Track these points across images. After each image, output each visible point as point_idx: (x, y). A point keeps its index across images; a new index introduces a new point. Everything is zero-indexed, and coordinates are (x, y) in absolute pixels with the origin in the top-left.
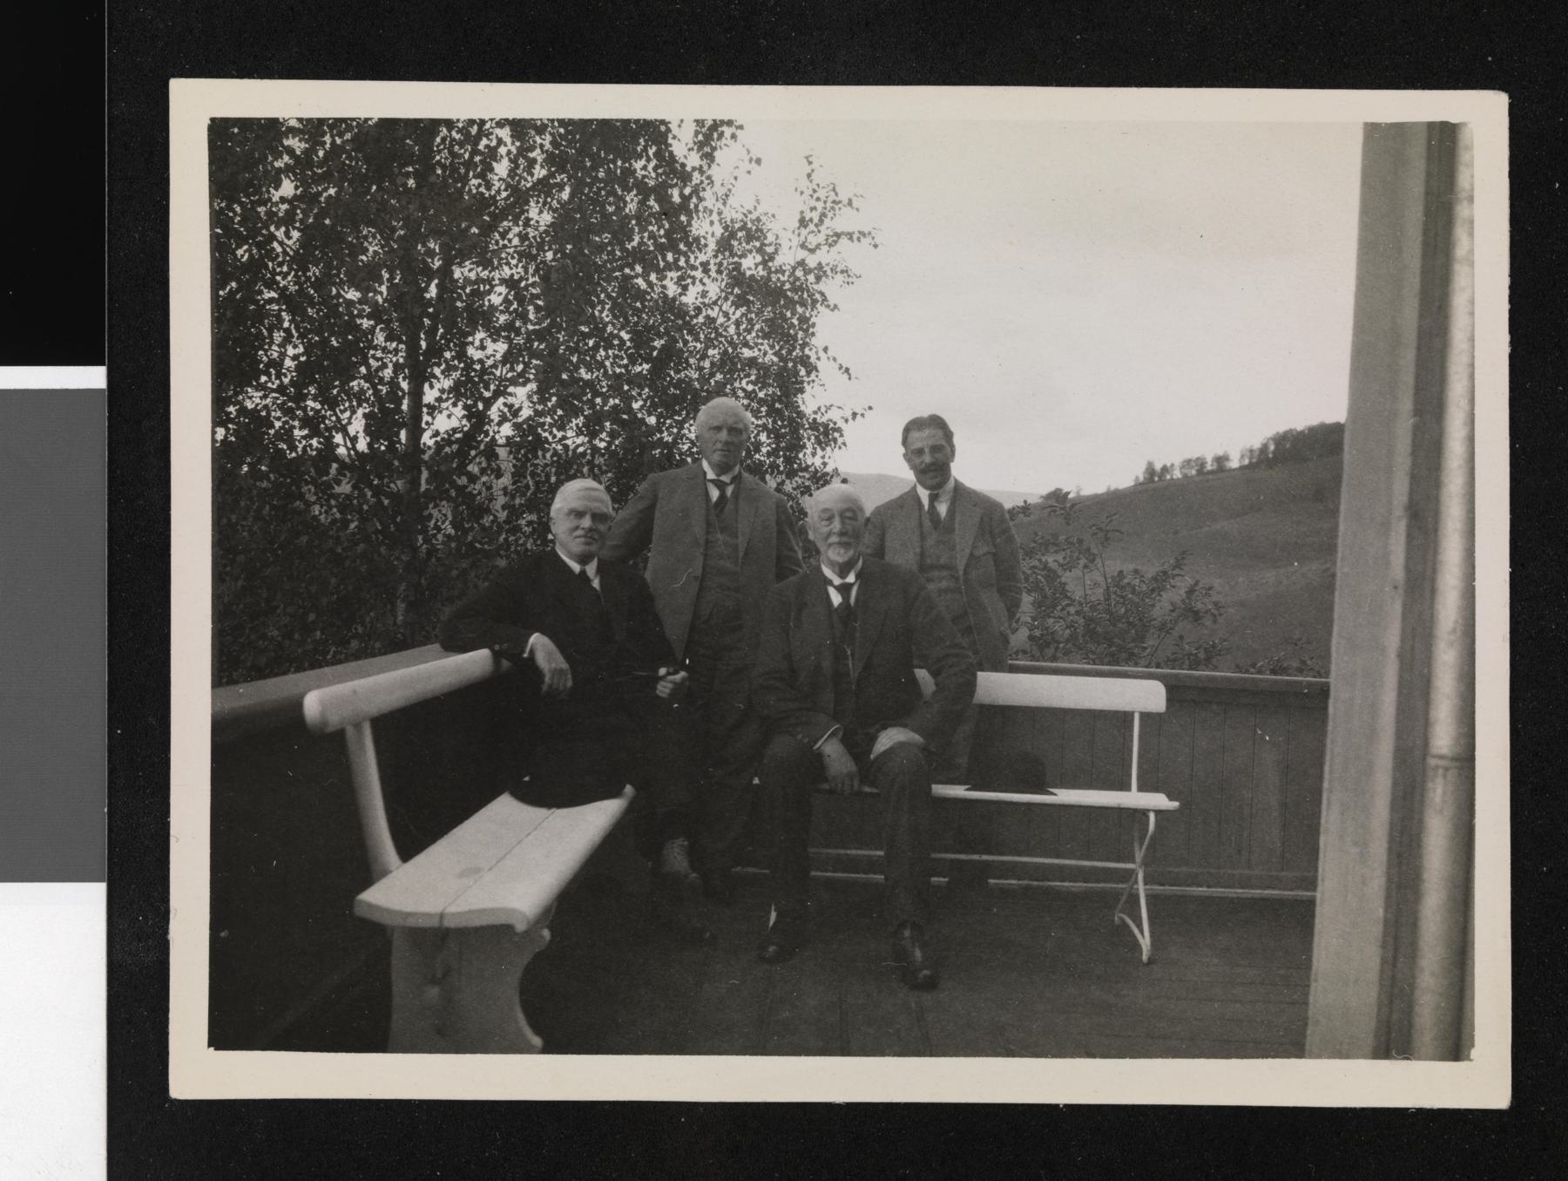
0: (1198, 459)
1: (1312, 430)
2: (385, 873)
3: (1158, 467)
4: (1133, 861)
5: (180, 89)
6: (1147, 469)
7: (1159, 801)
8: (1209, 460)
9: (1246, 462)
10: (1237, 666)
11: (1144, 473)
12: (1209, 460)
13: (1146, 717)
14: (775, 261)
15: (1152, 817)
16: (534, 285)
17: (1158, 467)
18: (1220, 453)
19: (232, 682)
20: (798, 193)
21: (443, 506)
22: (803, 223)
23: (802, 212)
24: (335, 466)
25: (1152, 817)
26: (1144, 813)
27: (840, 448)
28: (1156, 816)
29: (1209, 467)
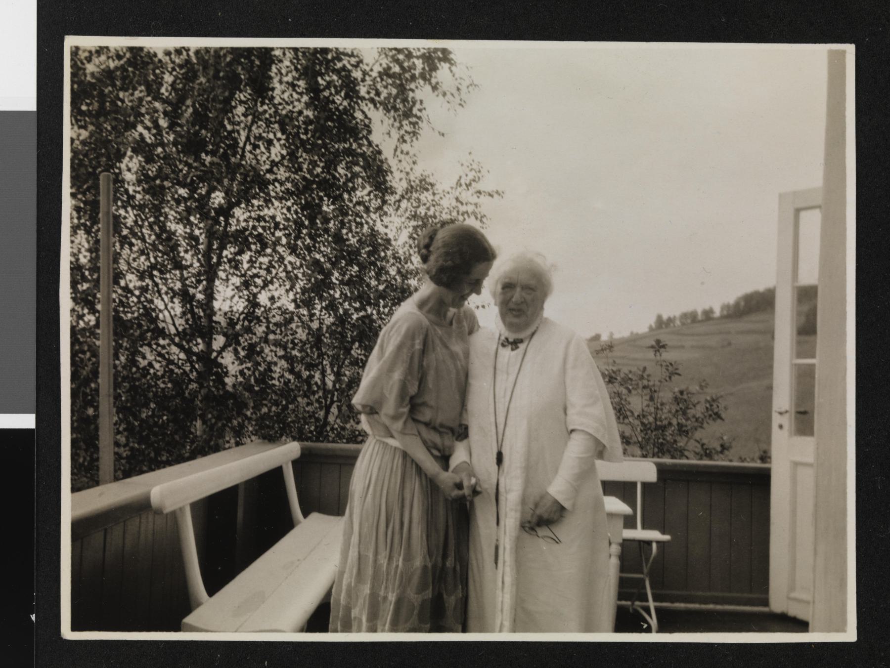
2: (199, 604)
4: (642, 573)
5: (850, 635)
7: (654, 535)
8: (699, 312)
9: (725, 313)
10: (740, 458)
12: (699, 312)
13: (644, 485)
14: (398, 191)
15: (654, 546)
16: (152, 172)
18: (707, 307)
21: (272, 299)
23: (460, 177)
25: (654, 546)
26: (649, 543)
27: (677, 369)
28: (658, 548)
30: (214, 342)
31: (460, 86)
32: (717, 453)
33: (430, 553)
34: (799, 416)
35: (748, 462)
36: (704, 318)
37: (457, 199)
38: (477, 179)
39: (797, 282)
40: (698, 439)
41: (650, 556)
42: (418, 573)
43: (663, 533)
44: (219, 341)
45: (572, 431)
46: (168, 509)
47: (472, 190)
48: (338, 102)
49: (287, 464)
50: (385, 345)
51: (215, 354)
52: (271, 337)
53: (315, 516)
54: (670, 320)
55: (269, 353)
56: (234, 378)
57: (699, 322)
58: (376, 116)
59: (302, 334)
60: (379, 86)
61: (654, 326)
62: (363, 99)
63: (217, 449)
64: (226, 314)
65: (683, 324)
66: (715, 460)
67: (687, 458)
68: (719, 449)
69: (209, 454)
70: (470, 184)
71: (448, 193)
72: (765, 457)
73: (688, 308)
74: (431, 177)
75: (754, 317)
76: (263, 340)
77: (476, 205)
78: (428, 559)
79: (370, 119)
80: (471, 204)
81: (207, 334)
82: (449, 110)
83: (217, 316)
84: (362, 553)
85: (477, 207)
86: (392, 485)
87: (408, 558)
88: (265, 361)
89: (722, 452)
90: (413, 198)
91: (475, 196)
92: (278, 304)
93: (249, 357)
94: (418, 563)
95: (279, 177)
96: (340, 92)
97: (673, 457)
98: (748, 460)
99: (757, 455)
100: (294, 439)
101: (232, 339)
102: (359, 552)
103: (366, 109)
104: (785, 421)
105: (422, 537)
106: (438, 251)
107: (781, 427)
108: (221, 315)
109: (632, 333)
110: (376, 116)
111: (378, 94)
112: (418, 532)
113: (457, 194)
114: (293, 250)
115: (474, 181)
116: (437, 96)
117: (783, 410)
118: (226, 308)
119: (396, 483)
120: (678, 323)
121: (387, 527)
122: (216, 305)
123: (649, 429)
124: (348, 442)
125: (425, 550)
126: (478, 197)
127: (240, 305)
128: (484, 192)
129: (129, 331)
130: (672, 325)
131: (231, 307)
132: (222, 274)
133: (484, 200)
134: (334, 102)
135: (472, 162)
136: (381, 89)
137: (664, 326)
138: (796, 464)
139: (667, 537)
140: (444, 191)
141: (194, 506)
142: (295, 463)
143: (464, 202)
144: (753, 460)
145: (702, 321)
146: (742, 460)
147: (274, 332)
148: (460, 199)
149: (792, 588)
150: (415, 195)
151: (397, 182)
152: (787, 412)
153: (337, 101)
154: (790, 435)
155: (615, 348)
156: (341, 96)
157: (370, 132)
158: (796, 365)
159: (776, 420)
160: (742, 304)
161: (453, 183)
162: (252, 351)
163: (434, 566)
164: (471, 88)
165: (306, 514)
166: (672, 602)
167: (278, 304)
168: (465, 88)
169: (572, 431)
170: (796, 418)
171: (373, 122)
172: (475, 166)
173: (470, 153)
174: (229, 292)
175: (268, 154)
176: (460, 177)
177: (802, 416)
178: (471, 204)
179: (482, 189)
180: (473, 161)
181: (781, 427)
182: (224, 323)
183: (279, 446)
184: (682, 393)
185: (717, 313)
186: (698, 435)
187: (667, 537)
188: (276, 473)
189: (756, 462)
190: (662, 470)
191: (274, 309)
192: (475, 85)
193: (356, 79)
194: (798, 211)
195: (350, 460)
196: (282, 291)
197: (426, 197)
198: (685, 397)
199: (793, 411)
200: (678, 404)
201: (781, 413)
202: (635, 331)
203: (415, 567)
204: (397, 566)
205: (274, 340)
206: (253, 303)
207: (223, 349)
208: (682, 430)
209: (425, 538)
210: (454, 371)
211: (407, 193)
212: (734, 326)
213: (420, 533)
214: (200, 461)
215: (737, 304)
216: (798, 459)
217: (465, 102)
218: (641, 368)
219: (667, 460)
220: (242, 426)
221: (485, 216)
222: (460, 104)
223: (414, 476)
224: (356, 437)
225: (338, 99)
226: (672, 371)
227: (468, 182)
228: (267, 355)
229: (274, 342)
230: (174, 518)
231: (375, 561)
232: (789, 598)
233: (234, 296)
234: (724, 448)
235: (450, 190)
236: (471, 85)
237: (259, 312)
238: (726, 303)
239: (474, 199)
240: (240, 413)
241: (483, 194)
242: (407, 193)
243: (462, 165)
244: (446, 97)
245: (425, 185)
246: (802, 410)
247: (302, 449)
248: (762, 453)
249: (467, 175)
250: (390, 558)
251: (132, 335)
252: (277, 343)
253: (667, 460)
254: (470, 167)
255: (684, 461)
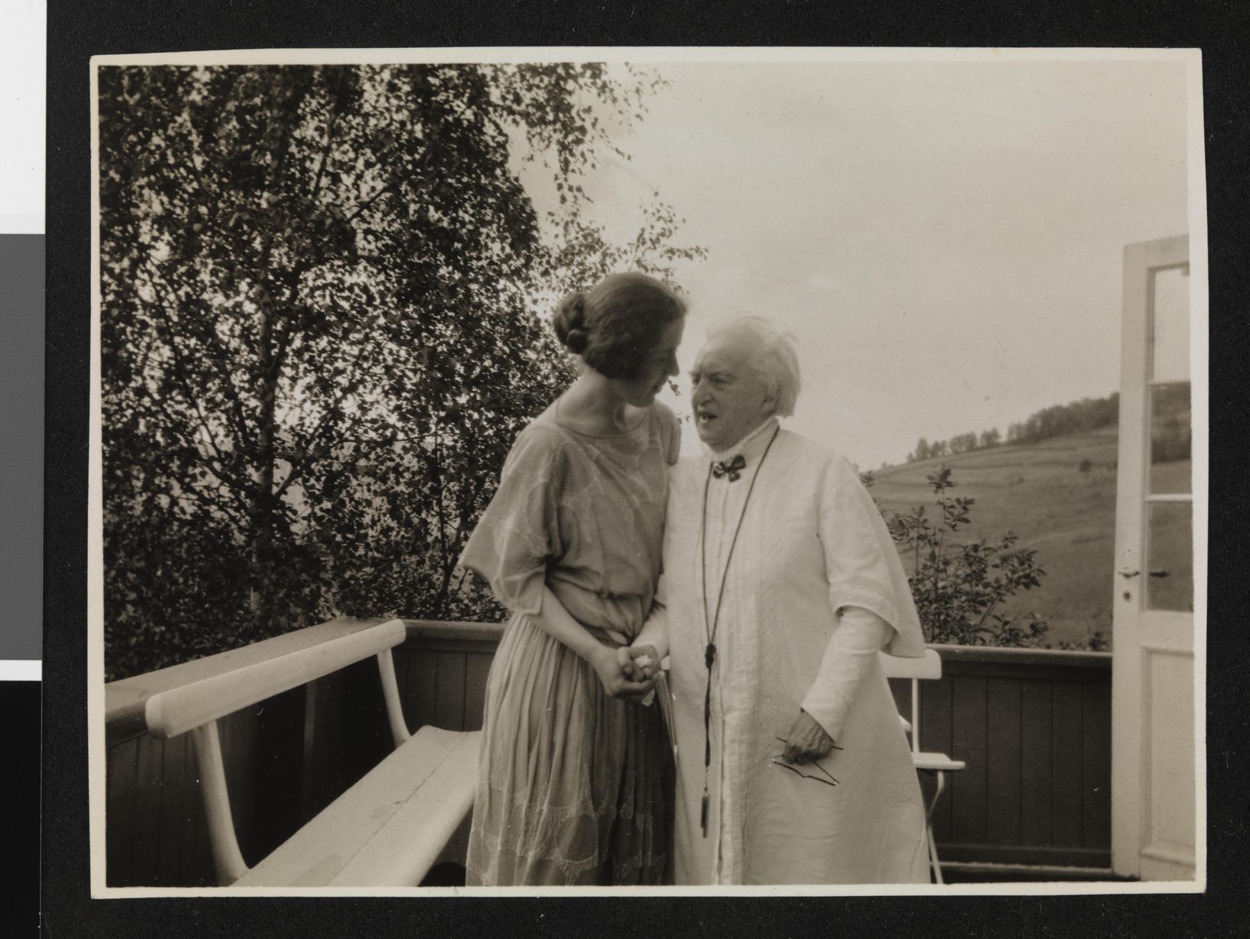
0: (968, 436)
1: (1076, 406)
3: (930, 443)
5: (1197, 884)
6: (920, 447)
8: (979, 435)
9: (1015, 436)
11: (917, 451)
12: (979, 435)
13: (922, 683)
15: (941, 776)
17: (930, 443)
18: (989, 429)
19: (120, 676)
20: (642, 210)
21: (363, 407)
22: (641, 239)
23: (643, 230)
24: (176, 523)
25: (941, 776)
28: (945, 778)
29: (979, 444)
30: (275, 471)
31: (640, 87)
32: (1027, 637)
33: (595, 797)
34: (1154, 579)
35: (1072, 649)
36: (985, 443)
37: (638, 262)
38: (668, 233)
39: (1152, 378)
40: (998, 614)
41: (934, 795)
42: (574, 824)
43: (953, 757)
44: (283, 470)
45: (841, 611)
46: (177, 728)
47: (660, 249)
48: (459, 110)
49: (384, 652)
50: (556, 484)
51: (275, 490)
52: (362, 462)
53: (427, 732)
54: (938, 447)
55: (361, 487)
56: (305, 522)
57: (978, 449)
58: (517, 133)
59: (410, 461)
60: (518, 85)
61: (914, 455)
62: (495, 107)
63: (276, 631)
64: (292, 428)
65: (956, 453)
66: (1022, 646)
67: (984, 642)
68: (1029, 632)
69: (266, 638)
70: (658, 240)
71: (625, 252)
72: (1100, 639)
73: (962, 431)
74: (601, 232)
75: (1056, 443)
76: (349, 467)
77: (666, 270)
78: (591, 807)
79: (506, 135)
80: (659, 270)
81: (265, 459)
82: (621, 123)
83: (281, 431)
84: (494, 787)
85: (667, 275)
86: (540, 681)
87: (557, 801)
88: (352, 499)
89: (1034, 635)
90: (575, 263)
91: (665, 257)
92: (372, 415)
93: (329, 492)
94: (573, 810)
95: (373, 227)
96: (463, 94)
97: (963, 641)
98: (1072, 646)
99: (1087, 639)
100: (400, 614)
101: (301, 468)
102: (490, 785)
103: (500, 122)
104: (1134, 587)
105: (582, 769)
106: (601, 324)
107: (1127, 596)
108: (285, 431)
109: (884, 465)
110: (517, 133)
111: (518, 100)
112: (575, 761)
113: (639, 254)
114: (396, 337)
115: (663, 235)
116: (605, 102)
117: (1131, 570)
118: (293, 421)
119: (547, 678)
120: (949, 450)
121: (530, 749)
122: (279, 415)
123: (926, 599)
124: (479, 620)
125: (587, 792)
126: (670, 258)
127: (313, 417)
128: (679, 250)
129: (139, 454)
130: (940, 454)
131: (301, 419)
132: (288, 371)
133: (679, 263)
134: (452, 111)
135: (659, 207)
136: (523, 93)
137: (928, 455)
138: (1151, 652)
139: (959, 764)
140: (619, 250)
141: (222, 722)
142: (397, 651)
143: (649, 267)
144: (1080, 646)
145: (982, 448)
146: (1064, 646)
147: (366, 456)
148: (644, 263)
149: (1146, 841)
150: (578, 259)
151: (549, 237)
152: (1137, 574)
153: (456, 108)
154: (1142, 609)
155: (875, 482)
156: (462, 101)
157: (506, 157)
158: (1150, 503)
159: (1120, 585)
160: (1039, 424)
161: (634, 238)
162: (334, 485)
163: (603, 820)
164: (657, 87)
165: (413, 729)
166: (966, 861)
167: (372, 415)
168: (650, 87)
169: (841, 611)
170: (1151, 584)
171: (510, 140)
172: (664, 214)
173: (656, 194)
174: (298, 394)
175: (356, 192)
176: (643, 230)
177: (1159, 580)
178: (659, 270)
179: (675, 247)
180: (661, 205)
181: (1127, 596)
182: (290, 441)
183: (380, 623)
184: (976, 548)
185: (1004, 437)
186: (999, 608)
187: (959, 764)
188: (369, 666)
189: (1084, 649)
190: (948, 661)
191: (366, 421)
192: (665, 82)
193: (484, 76)
194: (1153, 271)
195: (488, 645)
196: (378, 393)
197: (593, 259)
198: (981, 554)
199: (1146, 574)
200: (970, 565)
201: (1127, 576)
202: (889, 463)
203: (568, 817)
204: (541, 811)
205: (366, 466)
206: (335, 414)
207: (288, 483)
208: (976, 601)
209: (586, 772)
210: (630, 512)
211: (566, 255)
212: (1025, 454)
213: (579, 763)
214: (254, 648)
215: (1031, 425)
216: (1153, 645)
217: (647, 111)
218: (917, 508)
219: (953, 646)
220: (316, 595)
221: (680, 287)
222: (638, 116)
223: (575, 669)
224: (493, 611)
225: (459, 105)
226: (961, 513)
227: (654, 238)
228: (356, 491)
229: (365, 470)
230: (190, 743)
231: (512, 800)
232: (1141, 855)
233: (304, 401)
234: (1036, 630)
235: (628, 249)
236: (657, 82)
237: (343, 426)
238: (1016, 422)
239: (664, 263)
240: (316, 578)
241: (677, 254)
242: (566, 255)
243: (645, 211)
244: (617, 104)
245: (592, 243)
246: (1159, 570)
247: (408, 630)
248: (1093, 636)
249: (652, 227)
250: (532, 798)
251: (145, 460)
252: (370, 472)
253: (953, 646)
254: (657, 215)
255: (978, 648)
